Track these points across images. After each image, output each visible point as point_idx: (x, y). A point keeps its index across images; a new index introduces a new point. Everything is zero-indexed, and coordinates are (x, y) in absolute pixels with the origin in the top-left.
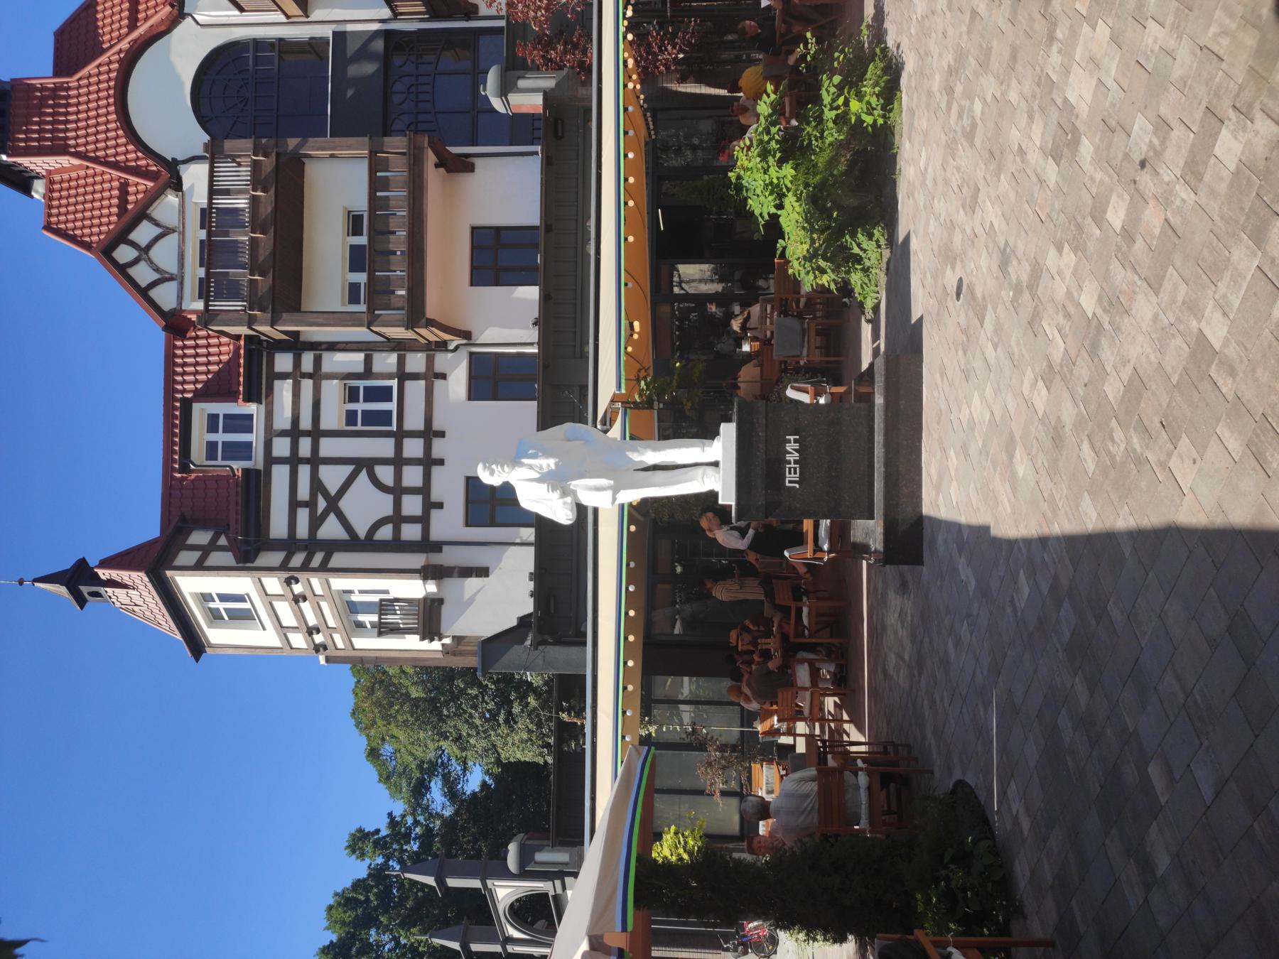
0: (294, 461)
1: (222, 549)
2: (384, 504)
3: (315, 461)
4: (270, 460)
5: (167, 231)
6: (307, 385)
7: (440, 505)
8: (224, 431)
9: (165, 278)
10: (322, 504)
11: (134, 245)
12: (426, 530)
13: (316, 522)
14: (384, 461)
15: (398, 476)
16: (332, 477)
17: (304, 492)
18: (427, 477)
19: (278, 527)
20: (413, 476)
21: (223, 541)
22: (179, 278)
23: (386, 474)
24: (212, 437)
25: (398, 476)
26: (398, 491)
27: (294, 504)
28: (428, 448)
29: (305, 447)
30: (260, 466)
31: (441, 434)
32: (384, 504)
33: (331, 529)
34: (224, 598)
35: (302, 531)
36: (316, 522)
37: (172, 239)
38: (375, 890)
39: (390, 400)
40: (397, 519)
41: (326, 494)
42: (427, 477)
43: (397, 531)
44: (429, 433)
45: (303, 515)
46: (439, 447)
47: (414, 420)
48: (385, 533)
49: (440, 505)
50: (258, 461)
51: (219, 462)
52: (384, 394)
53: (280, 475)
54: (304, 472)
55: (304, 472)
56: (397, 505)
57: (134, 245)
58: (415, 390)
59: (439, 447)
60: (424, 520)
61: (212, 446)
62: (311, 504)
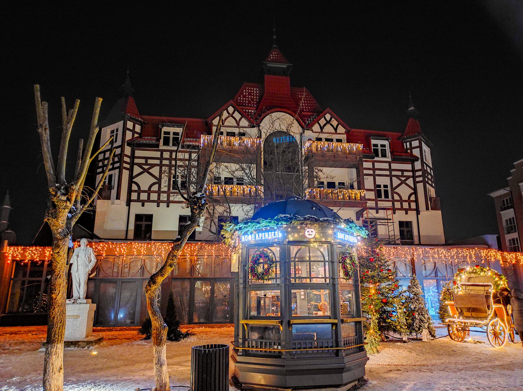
0: (161, 158)
1: (133, 135)
2: (144, 187)
3: (161, 165)
4: (162, 151)
5: (336, 129)
6: (387, 173)
7: (406, 213)
8: (381, 149)
9: (322, 128)
10: (146, 167)
11: (234, 112)
12: (135, 201)
13: (140, 165)
14: (160, 187)
15: (154, 192)
16: (155, 171)
17: (150, 161)
18: (153, 201)
19: (138, 153)
20: (406, 205)
21: (136, 135)
22: (322, 132)
23: (155, 188)
24: (171, 134)
25: (154, 192)
26: (149, 192)
27: (147, 158)
28: (163, 202)
29: (173, 162)
30: (161, 148)
31: (168, 206)
32: (144, 187)
33: (137, 170)
34: (117, 135)
35: (136, 161)
36: (140, 165)
37: (334, 131)
38: (62, 187)
39: (385, 198)
40: (139, 191)
41: (150, 168)
42: (153, 201)
43: (135, 191)
44: (168, 203)
45: (143, 161)
46: (163, 205)
47: (381, 204)
48: (134, 187)
49: (406, 213)
50: (162, 147)
51: (372, 148)
52: (386, 196)
53: (158, 154)
54: (157, 162)
55: (157, 162)
56: (144, 191)
57: (234, 112)
58: (389, 204)
59: (163, 205)
60: (138, 200)
61: (169, 133)
62: (146, 164)
